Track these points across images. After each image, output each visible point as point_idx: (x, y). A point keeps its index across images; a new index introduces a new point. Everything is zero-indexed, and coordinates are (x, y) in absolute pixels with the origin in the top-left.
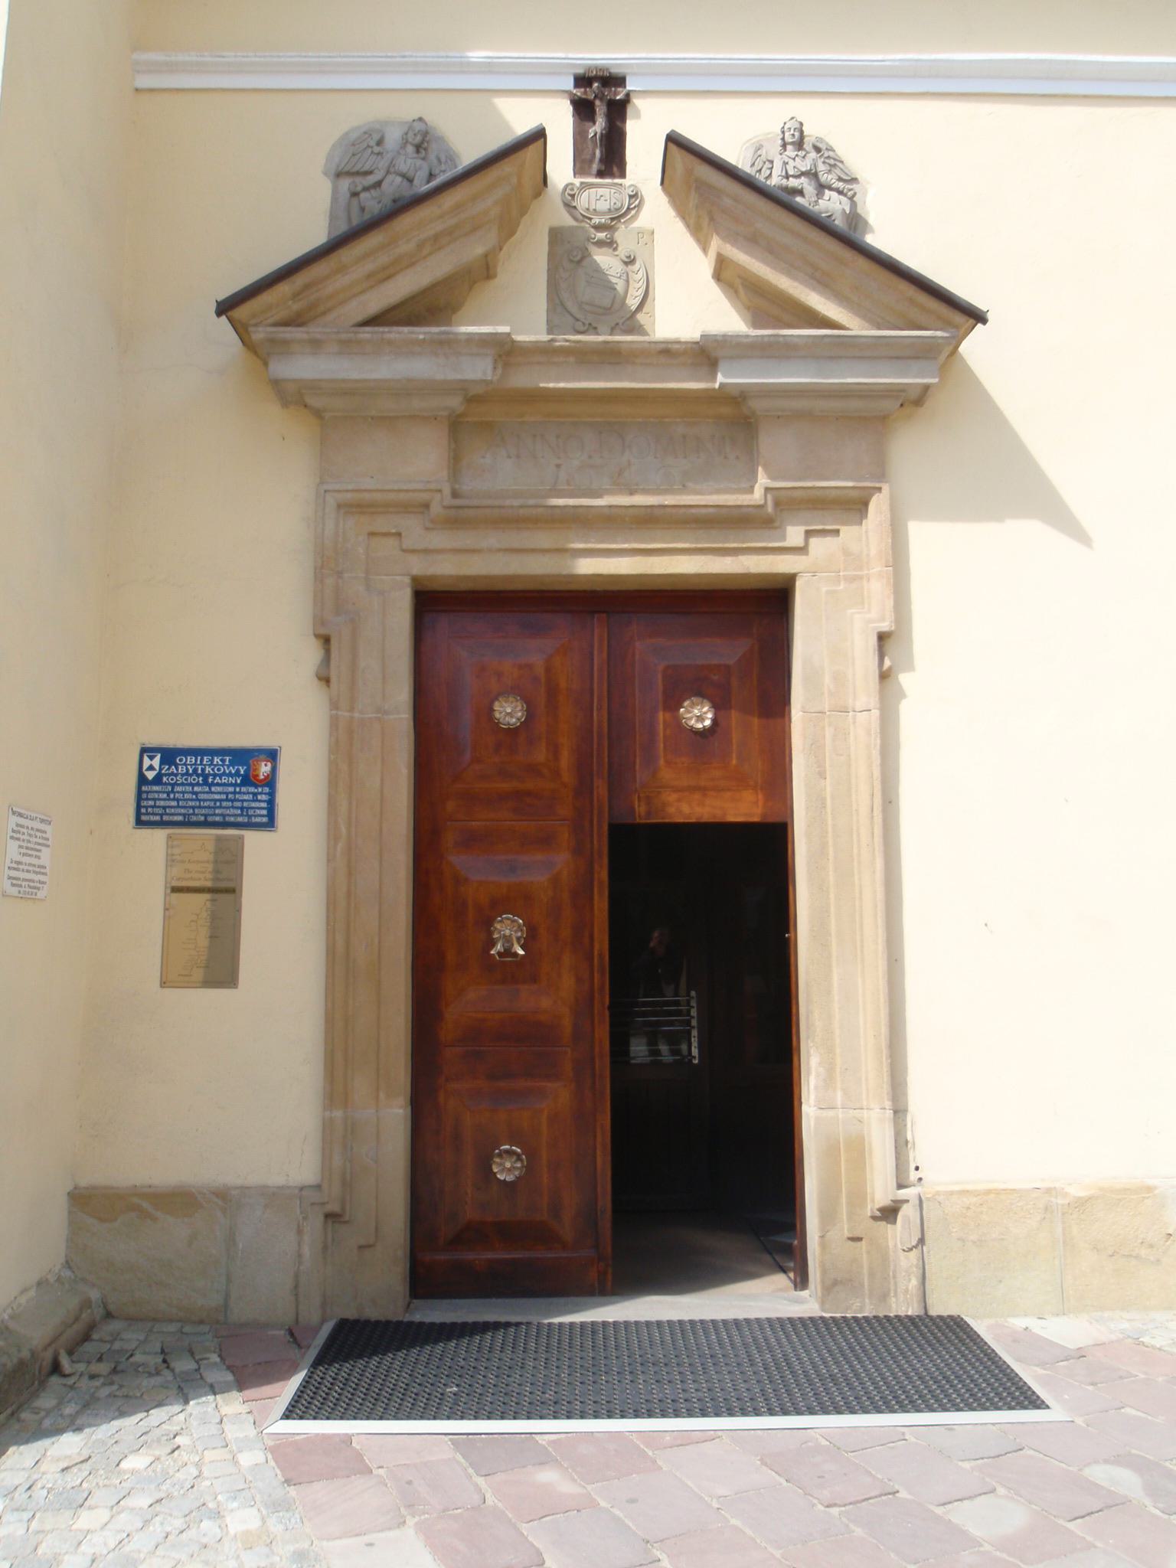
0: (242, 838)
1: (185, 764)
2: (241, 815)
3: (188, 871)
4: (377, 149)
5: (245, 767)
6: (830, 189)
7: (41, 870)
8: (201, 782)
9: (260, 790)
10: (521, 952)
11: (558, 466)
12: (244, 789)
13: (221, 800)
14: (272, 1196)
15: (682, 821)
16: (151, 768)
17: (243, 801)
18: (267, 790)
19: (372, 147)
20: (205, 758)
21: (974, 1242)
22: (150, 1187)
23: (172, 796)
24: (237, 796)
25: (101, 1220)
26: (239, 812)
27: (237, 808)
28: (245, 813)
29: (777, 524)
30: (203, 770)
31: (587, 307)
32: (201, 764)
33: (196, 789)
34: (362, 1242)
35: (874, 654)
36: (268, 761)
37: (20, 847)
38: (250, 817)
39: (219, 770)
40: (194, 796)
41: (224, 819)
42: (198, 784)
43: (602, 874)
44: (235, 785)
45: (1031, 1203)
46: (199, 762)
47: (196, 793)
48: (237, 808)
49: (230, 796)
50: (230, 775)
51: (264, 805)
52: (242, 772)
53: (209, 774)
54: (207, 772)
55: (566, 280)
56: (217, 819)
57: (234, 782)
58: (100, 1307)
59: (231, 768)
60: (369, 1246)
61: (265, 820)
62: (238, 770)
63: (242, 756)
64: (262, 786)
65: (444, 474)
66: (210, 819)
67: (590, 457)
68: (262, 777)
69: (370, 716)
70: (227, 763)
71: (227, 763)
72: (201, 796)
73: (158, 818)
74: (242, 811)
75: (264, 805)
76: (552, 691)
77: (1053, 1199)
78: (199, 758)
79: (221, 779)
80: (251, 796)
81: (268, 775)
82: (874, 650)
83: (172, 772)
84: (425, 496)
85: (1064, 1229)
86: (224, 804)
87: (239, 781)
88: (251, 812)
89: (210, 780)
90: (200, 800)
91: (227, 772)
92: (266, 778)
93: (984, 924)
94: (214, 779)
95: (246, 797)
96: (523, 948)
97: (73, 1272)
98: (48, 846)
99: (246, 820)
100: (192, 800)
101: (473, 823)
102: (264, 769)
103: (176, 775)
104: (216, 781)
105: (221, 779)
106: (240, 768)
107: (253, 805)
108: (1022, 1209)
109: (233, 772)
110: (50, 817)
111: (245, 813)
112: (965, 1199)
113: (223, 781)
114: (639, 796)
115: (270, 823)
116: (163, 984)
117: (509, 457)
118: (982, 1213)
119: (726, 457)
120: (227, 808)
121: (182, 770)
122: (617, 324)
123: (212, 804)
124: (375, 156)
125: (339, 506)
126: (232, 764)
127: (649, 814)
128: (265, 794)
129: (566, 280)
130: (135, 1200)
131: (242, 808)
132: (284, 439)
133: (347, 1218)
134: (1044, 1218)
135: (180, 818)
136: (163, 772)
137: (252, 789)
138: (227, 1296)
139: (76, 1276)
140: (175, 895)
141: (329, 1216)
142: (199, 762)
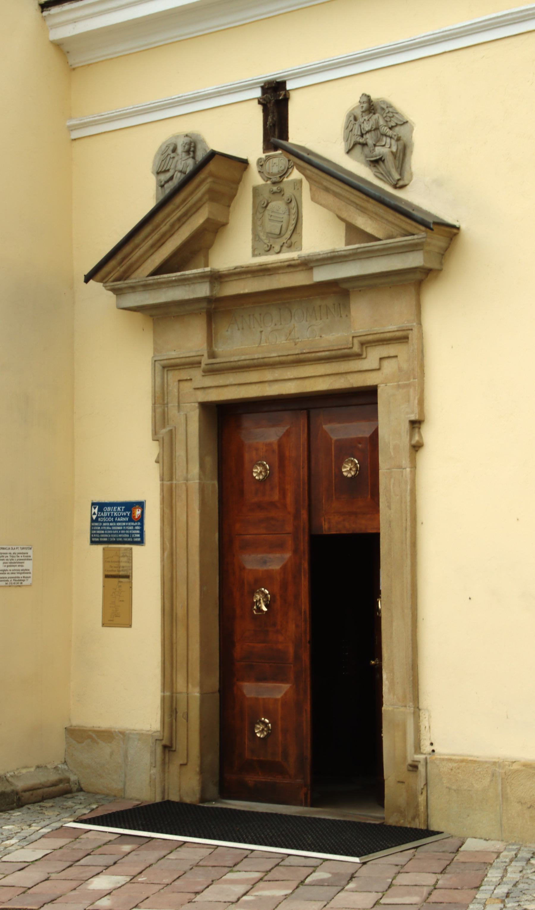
0: (131, 549)
1: (107, 511)
2: (129, 537)
3: (111, 567)
4: (172, 155)
5: (130, 512)
6: (386, 136)
7: (26, 571)
8: (112, 521)
9: (136, 524)
10: (265, 609)
11: (261, 332)
12: (129, 524)
13: (120, 530)
14: (141, 736)
15: (335, 533)
16: (94, 514)
17: (129, 530)
18: (139, 524)
19: (170, 154)
20: (114, 508)
21: (455, 791)
22: (99, 727)
23: (102, 528)
24: (127, 527)
25: (79, 742)
26: (128, 536)
27: (127, 534)
28: (131, 536)
29: (364, 356)
30: (113, 514)
31: (269, 235)
32: (113, 511)
33: (111, 524)
34: (182, 762)
35: (407, 434)
36: (139, 508)
37: (4, 563)
38: (133, 538)
39: (119, 514)
40: (110, 528)
41: (123, 539)
42: (111, 522)
43: (306, 565)
44: (126, 522)
45: (485, 770)
46: (112, 510)
47: (111, 526)
48: (127, 534)
49: (124, 528)
50: (124, 516)
51: (138, 532)
52: (128, 515)
53: (116, 517)
54: (115, 515)
55: (260, 218)
56: (120, 539)
57: (125, 520)
58: (76, 784)
59: (124, 513)
60: (186, 764)
61: (139, 539)
62: (127, 514)
63: (129, 506)
64: (137, 522)
65: (205, 345)
66: (118, 539)
67: (275, 325)
68: (137, 517)
69: (182, 482)
70: (123, 510)
71: (123, 510)
72: (114, 528)
73: (97, 539)
74: (129, 535)
75: (138, 532)
76: (282, 458)
77: (497, 769)
78: (112, 508)
79: (120, 519)
80: (132, 527)
81: (140, 516)
82: (407, 432)
83: (102, 516)
84: (197, 359)
85: (502, 788)
86: (122, 532)
87: (127, 520)
88: (133, 536)
89: (116, 519)
90: (113, 530)
91: (123, 515)
92: (139, 517)
93: (472, 599)
94: (118, 519)
95: (130, 528)
96: (266, 606)
97: (68, 767)
98: (31, 559)
99: (131, 540)
100: (109, 530)
101: (248, 536)
102: (138, 512)
103: (103, 517)
104: (118, 520)
105: (120, 519)
106: (128, 512)
107: (134, 532)
108: (480, 773)
109: (125, 515)
110: (31, 546)
111: (131, 536)
112: (450, 764)
113: (121, 520)
114: (325, 519)
115: (141, 542)
116: (104, 625)
117: (239, 329)
118: (459, 773)
119: (341, 317)
120: (123, 534)
121: (105, 514)
122: (284, 243)
123: (117, 532)
124: (172, 159)
125: (164, 367)
126: (125, 510)
127: (329, 528)
128: (139, 526)
129: (260, 218)
130: (90, 733)
131: (129, 534)
132: (143, 330)
133: (174, 749)
134: (492, 780)
135: (106, 539)
136: (99, 515)
137: (133, 524)
138: (125, 785)
139: (69, 769)
140: (107, 579)
141: (165, 747)
142: (112, 510)
